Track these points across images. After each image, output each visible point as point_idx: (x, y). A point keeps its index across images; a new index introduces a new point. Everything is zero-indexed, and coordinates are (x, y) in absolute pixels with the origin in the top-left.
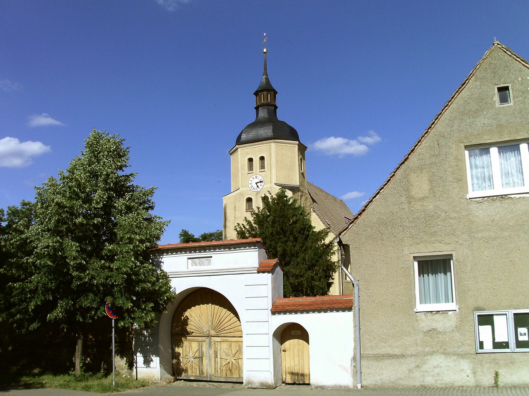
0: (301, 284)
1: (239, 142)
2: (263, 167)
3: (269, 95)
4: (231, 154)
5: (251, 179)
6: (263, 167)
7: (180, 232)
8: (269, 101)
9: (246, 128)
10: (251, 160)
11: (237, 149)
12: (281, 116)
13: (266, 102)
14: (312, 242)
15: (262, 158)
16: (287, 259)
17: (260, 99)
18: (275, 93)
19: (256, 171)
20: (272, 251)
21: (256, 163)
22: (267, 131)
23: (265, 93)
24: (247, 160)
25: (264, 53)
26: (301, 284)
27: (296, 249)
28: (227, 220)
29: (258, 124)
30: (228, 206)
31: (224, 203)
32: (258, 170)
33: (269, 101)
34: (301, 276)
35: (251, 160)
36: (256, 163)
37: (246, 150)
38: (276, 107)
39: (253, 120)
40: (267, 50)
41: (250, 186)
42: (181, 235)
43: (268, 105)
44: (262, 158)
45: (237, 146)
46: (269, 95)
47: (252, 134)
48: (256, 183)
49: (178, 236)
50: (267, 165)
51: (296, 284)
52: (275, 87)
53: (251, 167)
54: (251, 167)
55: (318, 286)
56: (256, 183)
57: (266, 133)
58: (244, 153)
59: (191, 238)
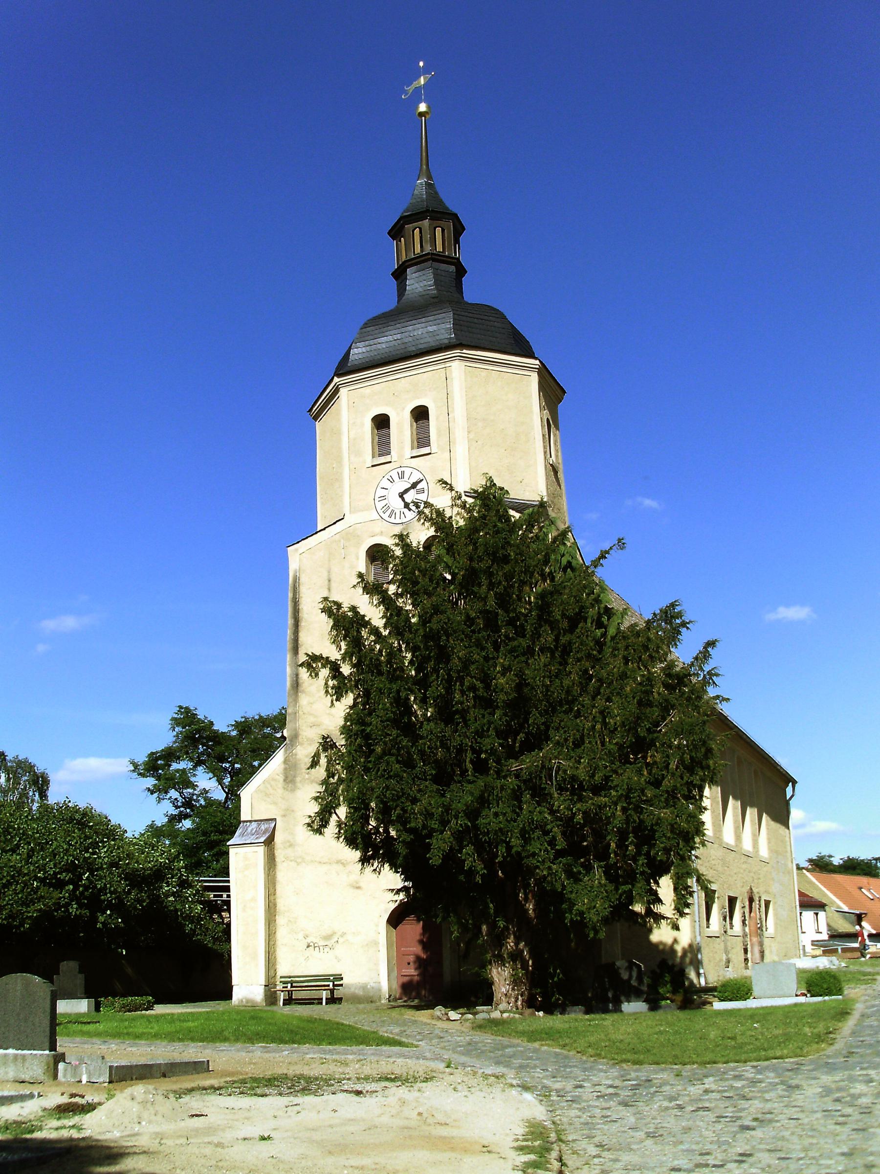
0: (596, 821)
1: (345, 368)
2: (422, 440)
3: (438, 231)
4: (316, 418)
5: (385, 483)
6: (422, 440)
7: (172, 712)
8: (439, 248)
9: (366, 325)
10: (382, 422)
11: (336, 390)
12: (474, 291)
13: (428, 248)
14: (626, 660)
15: (420, 414)
16: (535, 718)
17: (409, 245)
18: (459, 229)
19: (401, 456)
20: (473, 688)
21: (402, 429)
22: (440, 327)
23: (426, 222)
24: (368, 425)
25: (421, 114)
26: (596, 821)
27: (567, 682)
28: (303, 624)
29: (407, 311)
30: (303, 579)
31: (293, 566)
32: (408, 452)
33: (439, 248)
34: (597, 790)
35: (382, 422)
36: (402, 429)
37: (368, 391)
38: (461, 271)
39: (391, 303)
40: (429, 107)
41: (380, 505)
42: (176, 722)
43: (434, 258)
44: (420, 414)
45: (336, 380)
46: (438, 231)
47: (387, 340)
48: (401, 495)
49: (167, 723)
50: (439, 434)
51: (579, 817)
52: (452, 205)
53: (383, 446)
54: (383, 446)
55: (673, 827)
56: (401, 495)
57: (433, 334)
58: (357, 402)
59: (204, 729)
